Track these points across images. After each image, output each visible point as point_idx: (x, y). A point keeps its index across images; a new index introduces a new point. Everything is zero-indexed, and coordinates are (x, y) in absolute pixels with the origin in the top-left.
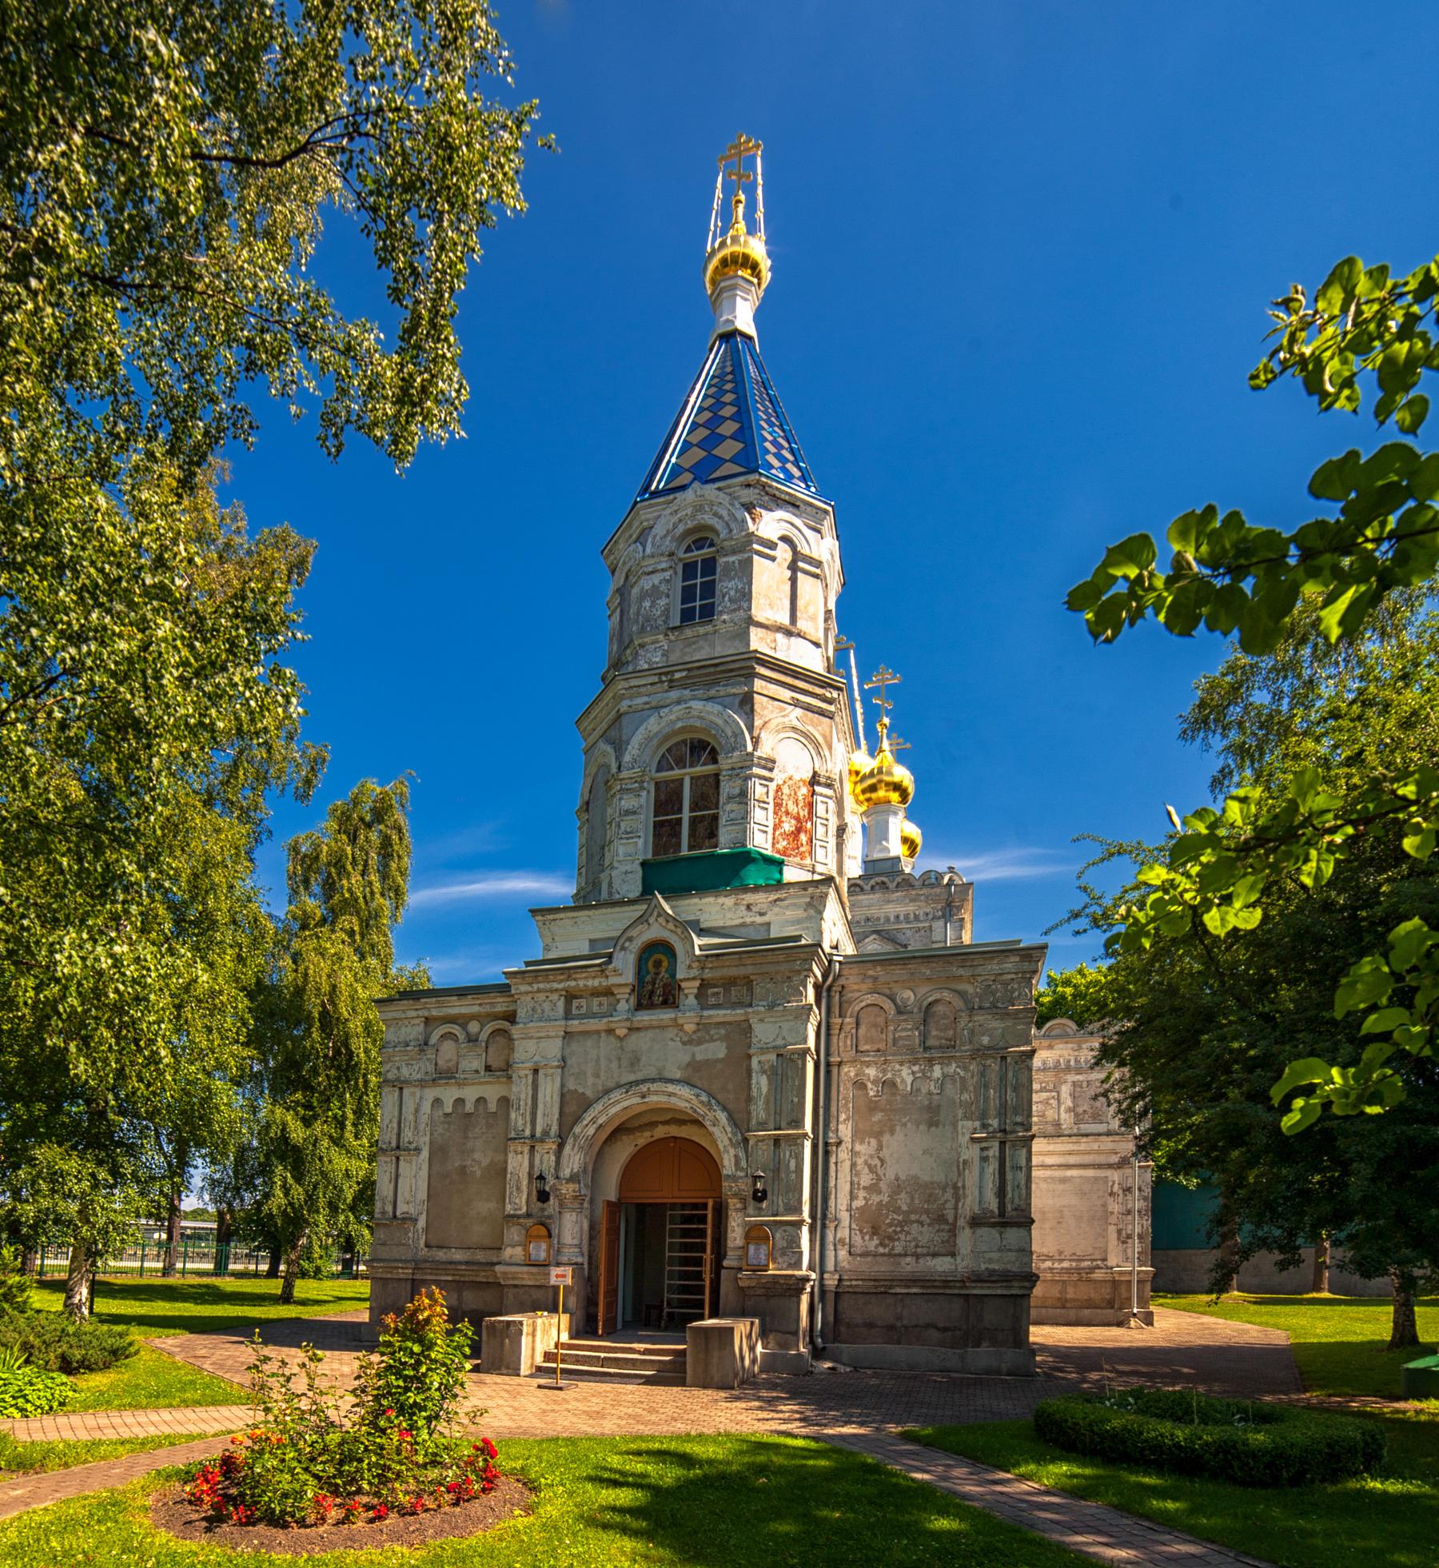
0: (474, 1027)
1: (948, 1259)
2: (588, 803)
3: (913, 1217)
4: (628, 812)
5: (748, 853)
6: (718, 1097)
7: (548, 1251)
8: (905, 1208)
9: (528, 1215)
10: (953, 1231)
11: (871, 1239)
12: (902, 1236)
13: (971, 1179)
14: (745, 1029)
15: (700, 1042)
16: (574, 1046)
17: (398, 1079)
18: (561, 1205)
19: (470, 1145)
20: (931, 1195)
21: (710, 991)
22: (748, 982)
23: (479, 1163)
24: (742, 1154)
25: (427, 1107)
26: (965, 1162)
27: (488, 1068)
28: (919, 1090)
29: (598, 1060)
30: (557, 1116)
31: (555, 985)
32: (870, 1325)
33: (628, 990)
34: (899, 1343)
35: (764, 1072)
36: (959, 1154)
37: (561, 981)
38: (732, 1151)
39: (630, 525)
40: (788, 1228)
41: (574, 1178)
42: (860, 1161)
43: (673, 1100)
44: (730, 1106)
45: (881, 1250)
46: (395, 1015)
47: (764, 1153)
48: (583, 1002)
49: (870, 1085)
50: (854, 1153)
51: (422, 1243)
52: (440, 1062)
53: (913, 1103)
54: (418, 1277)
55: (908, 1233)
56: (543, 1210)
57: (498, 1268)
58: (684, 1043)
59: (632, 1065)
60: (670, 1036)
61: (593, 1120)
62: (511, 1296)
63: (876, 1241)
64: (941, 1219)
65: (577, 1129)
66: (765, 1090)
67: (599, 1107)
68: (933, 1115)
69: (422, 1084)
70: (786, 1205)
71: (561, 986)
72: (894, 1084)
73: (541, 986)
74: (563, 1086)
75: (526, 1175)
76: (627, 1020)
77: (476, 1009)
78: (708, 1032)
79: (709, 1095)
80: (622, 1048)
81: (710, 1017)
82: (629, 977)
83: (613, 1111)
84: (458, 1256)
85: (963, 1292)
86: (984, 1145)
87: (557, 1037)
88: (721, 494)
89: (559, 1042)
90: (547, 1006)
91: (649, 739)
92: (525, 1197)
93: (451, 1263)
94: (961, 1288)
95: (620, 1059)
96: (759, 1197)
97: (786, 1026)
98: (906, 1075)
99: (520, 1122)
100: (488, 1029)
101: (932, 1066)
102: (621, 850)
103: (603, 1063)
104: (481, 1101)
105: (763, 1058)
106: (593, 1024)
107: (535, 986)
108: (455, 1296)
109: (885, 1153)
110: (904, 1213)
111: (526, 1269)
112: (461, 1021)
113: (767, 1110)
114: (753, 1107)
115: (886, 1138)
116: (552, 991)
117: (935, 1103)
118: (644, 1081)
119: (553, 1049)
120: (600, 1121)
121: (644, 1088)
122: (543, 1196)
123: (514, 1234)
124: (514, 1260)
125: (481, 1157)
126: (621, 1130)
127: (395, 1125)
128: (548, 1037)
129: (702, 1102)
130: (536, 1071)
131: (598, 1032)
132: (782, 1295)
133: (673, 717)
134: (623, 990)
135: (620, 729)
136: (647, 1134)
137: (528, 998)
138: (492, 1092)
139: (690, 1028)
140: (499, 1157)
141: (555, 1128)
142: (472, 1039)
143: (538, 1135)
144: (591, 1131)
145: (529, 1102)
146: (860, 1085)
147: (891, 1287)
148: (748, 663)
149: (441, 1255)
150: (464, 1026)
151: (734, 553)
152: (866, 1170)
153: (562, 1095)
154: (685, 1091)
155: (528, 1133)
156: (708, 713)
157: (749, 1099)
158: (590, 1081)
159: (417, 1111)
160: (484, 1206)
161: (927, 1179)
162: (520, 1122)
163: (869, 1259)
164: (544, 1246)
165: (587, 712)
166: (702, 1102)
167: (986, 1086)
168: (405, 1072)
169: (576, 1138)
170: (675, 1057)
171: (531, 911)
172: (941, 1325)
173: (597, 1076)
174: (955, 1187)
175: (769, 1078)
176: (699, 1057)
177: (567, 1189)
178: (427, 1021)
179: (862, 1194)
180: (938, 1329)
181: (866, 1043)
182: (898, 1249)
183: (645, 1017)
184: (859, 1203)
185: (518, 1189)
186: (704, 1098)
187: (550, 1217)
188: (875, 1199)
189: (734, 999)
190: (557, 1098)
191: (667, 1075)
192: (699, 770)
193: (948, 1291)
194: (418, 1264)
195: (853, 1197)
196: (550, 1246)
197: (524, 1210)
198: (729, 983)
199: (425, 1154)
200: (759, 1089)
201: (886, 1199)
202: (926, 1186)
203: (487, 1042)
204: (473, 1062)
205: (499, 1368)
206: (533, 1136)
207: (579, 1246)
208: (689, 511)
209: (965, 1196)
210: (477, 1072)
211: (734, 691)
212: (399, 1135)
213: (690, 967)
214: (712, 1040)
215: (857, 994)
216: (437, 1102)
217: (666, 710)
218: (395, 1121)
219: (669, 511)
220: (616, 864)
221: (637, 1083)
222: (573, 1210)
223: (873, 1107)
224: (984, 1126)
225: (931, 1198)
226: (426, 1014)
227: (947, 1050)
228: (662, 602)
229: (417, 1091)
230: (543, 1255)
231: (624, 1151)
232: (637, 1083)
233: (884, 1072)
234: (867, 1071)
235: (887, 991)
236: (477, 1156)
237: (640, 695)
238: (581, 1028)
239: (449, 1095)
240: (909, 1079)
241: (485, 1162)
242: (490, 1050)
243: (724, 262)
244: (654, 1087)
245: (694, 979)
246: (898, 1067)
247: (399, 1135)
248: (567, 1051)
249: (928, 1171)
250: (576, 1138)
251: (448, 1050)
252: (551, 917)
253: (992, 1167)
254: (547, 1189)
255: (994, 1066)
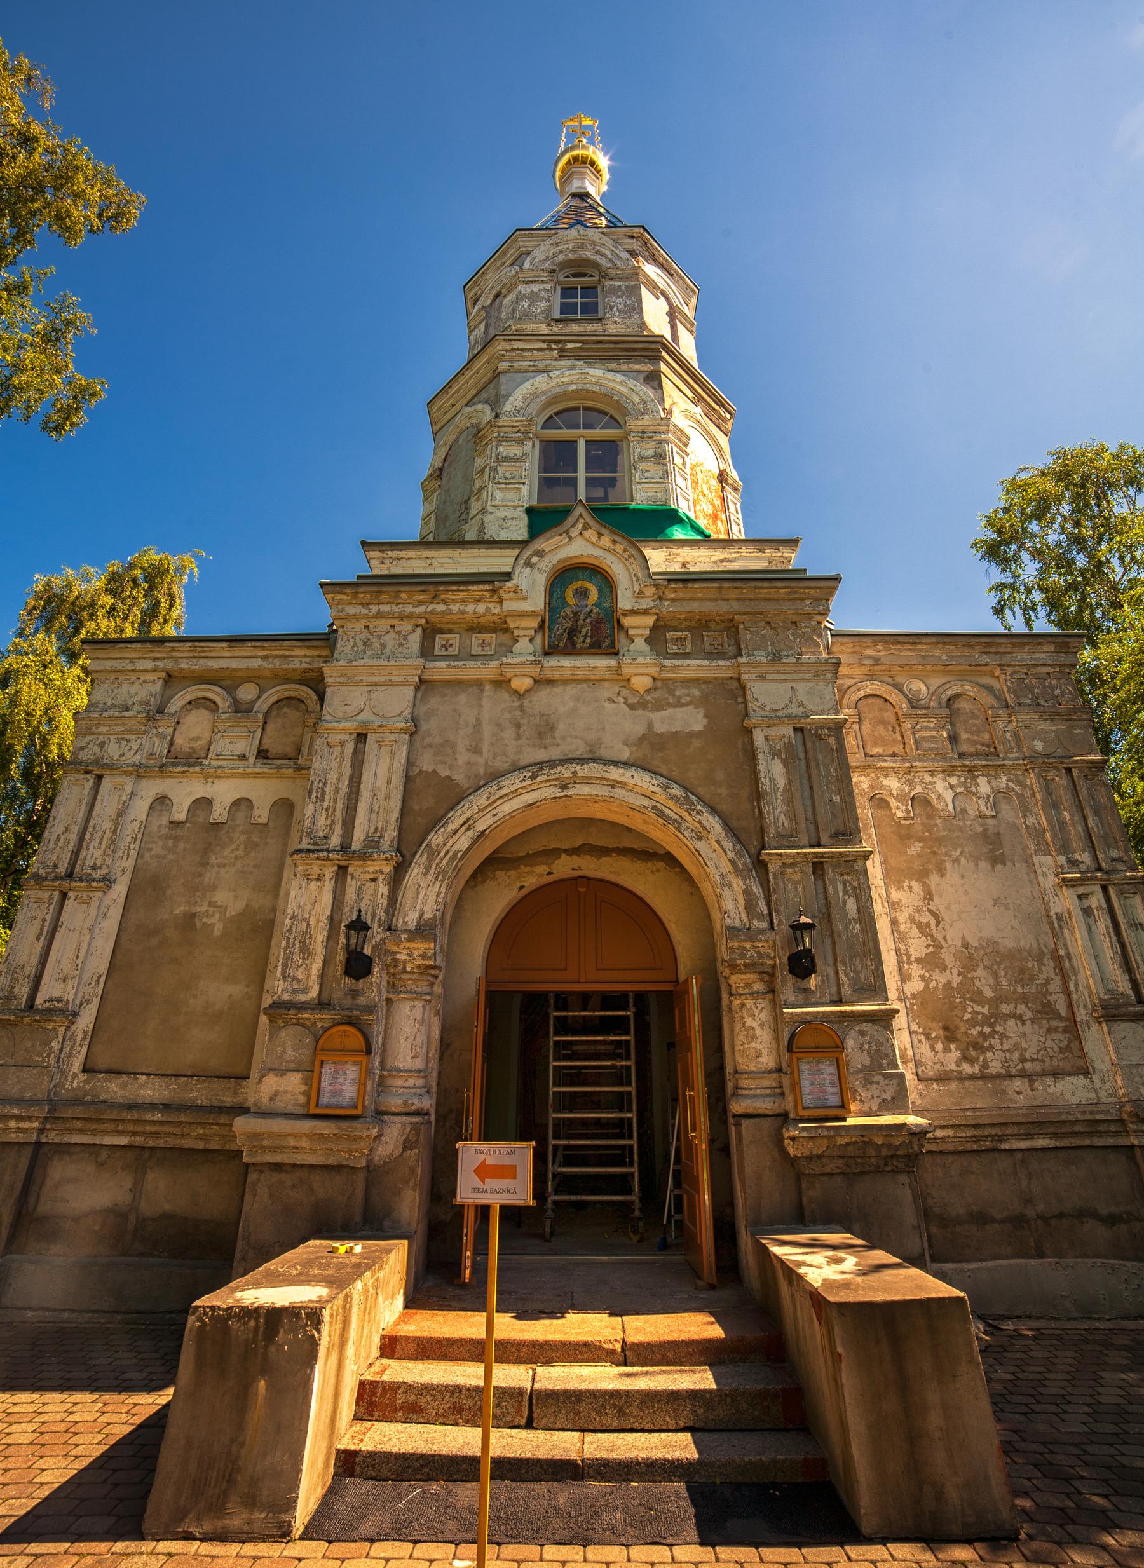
0: (246, 693)
1: (1080, 1080)
2: (441, 470)
3: (1005, 1008)
4: (507, 459)
5: (675, 511)
6: (701, 791)
7: (362, 1085)
8: (988, 993)
9: (322, 1004)
10: (1072, 1028)
11: (946, 1049)
12: (995, 1042)
13: (1077, 940)
14: (737, 690)
15: (659, 706)
16: (434, 702)
17: (97, 762)
18: (392, 987)
19: (209, 877)
20: (1022, 971)
21: (669, 635)
22: (731, 627)
23: (223, 909)
24: (757, 889)
25: (140, 809)
26: (1059, 917)
27: (262, 754)
28: (964, 811)
29: (478, 725)
30: (397, 813)
31: (409, 609)
32: (981, 1218)
33: (534, 623)
34: (1041, 1255)
35: (775, 754)
36: (1046, 904)
37: (421, 603)
38: (738, 884)
39: (504, 253)
40: (867, 1027)
41: (423, 931)
42: (903, 917)
43: (619, 793)
44: (723, 807)
45: (967, 1068)
46: (118, 664)
47: (795, 887)
48: (454, 639)
49: (893, 802)
50: (894, 905)
51: (77, 1063)
52: (179, 740)
53: (961, 829)
54: (52, 1137)
55: (1003, 1036)
56: (355, 993)
57: (241, 1124)
58: (632, 707)
59: (540, 735)
60: (606, 694)
61: (468, 824)
62: (263, 1192)
63: (955, 1054)
64: (1046, 1011)
65: (436, 839)
66: (781, 782)
67: (481, 800)
68: (993, 848)
69: (140, 772)
70: (854, 982)
71: (421, 609)
72: (927, 802)
73: (385, 608)
74: (410, 763)
75: (324, 921)
76: (534, 663)
77: (256, 663)
78: (671, 692)
79: (685, 788)
80: (522, 709)
81: (674, 668)
82: (537, 602)
83: (506, 808)
84: (150, 1090)
85: (1122, 1141)
86: (1081, 890)
87: (406, 684)
88: (605, 238)
89: (409, 693)
90: (390, 639)
91: (535, 395)
92: (317, 965)
93: (132, 1106)
94: (1117, 1133)
95: (518, 726)
96: (801, 965)
97: (801, 687)
98: (942, 790)
99: (322, 821)
100: (272, 695)
101: (975, 778)
102: (498, 495)
103: (487, 730)
104: (242, 804)
105: (772, 732)
106: (471, 670)
107: (374, 609)
108: (128, 1182)
109: (937, 904)
110: (989, 1001)
111: (307, 1126)
112: (228, 682)
113: (791, 813)
114: (766, 809)
115: (934, 880)
116: (402, 617)
117: (991, 831)
118: (564, 761)
119: (397, 703)
120: (481, 826)
121: (566, 772)
122: (358, 965)
123: (290, 1044)
124: (280, 1105)
125: (227, 897)
126: (496, 862)
127: (73, 837)
128: (389, 684)
129: (673, 798)
130: (361, 737)
131: (479, 684)
132: (878, 1171)
133: (565, 380)
134: (525, 623)
135: (498, 386)
136: (543, 869)
137: (359, 626)
138: (263, 792)
139: (641, 683)
140: (262, 901)
141: (391, 835)
142: (242, 710)
143: (356, 845)
144: (463, 842)
145: (344, 786)
146: (880, 802)
147: (1001, 1139)
148: (654, 346)
149: (114, 1089)
150: (230, 690)
151: (621, 279)
152: (915, 931)
153: (408, 779)
154: (642, 780)
155: (335, 841)
156: (609, 380)
157: (757, 796)
158: (463, 757)
159: (120, 813)
160: (220, 991)
161: (1010, 944)
162: (322, 821)
163: (953, 1086)
164: (352, 1072)
165: (448, 385)
166: (673, 798)
167: (1056, 805)
168: (113, 750)
169: (432, 854)
170: (620, 727)
171: (364, 544)
172: (1104, 1211)
173: (477, 750)
174: (1057, 959)
175: (785, 762)
176: (660, 728)
177: (411, 953)
178: (170, 679)
179: (916, 971)
180: (1101, 1219)
181: (875, 745)
182: (995, 1067)
183: (565, 664)
184: (915, 986)
185: (305, 949)
186: (677, 792)
187: (370, 1009)
188: (940, 979)
189: (708, 648)
190: (398, 781)
191: (605, 753)
192: (598, 433)
193: (1098, 1142)
194: (56, 1109)
195: (904, 978)
196: (367, 1072)
197: (314, 992)
198: (699, 626)
199: (120, 889)
200: (772, 780)
201: (956, 980)
202: (1012, 955)
203: (267, 715)
204: (237, 742)
205: (218, 1508)
206: (345, 847)
207: (423, 1073)
208: (570, 246)
209: (1075, 972)
210: (243, 757)
211: (638, 367)
212: (76, 854)
213: (640, 595)
214: (679, 704)
215: (850, 682)
216: (162, 802)
217: (557, 373)
218: (76, 828)
219: (549, 242)
220: (490, 509)
221: (552, 764)
222: (418, 995)
223: (905, 835)
224: (1073, 864)
225: (1023, 975)
226: (170, 665)
227: (987, 758)
228: (543, 304)
229: (129, 784)
230: (349, 1091)
231: (499, 897)
232: (552, 764)
233: (910, 783)
234: (886, 782)
235: (890, 680)
236: (221, 897)
237: (524, 359)
238: (449, 675)
239: (184, 792)
240: (948, 795)
241: (235, 907)
242: (270, 727)
243: (575, 159)
244: (584, 771)
245: (646, 612)
246: (927, 778)
247: (76, 854)
248: (422, 710)
249: (1013, 935)
250: (432, 854)
251: (196, 725)
252: (394, 554)
253: (1102, 924)
254: (367, 950)
255: (1062, 781)
